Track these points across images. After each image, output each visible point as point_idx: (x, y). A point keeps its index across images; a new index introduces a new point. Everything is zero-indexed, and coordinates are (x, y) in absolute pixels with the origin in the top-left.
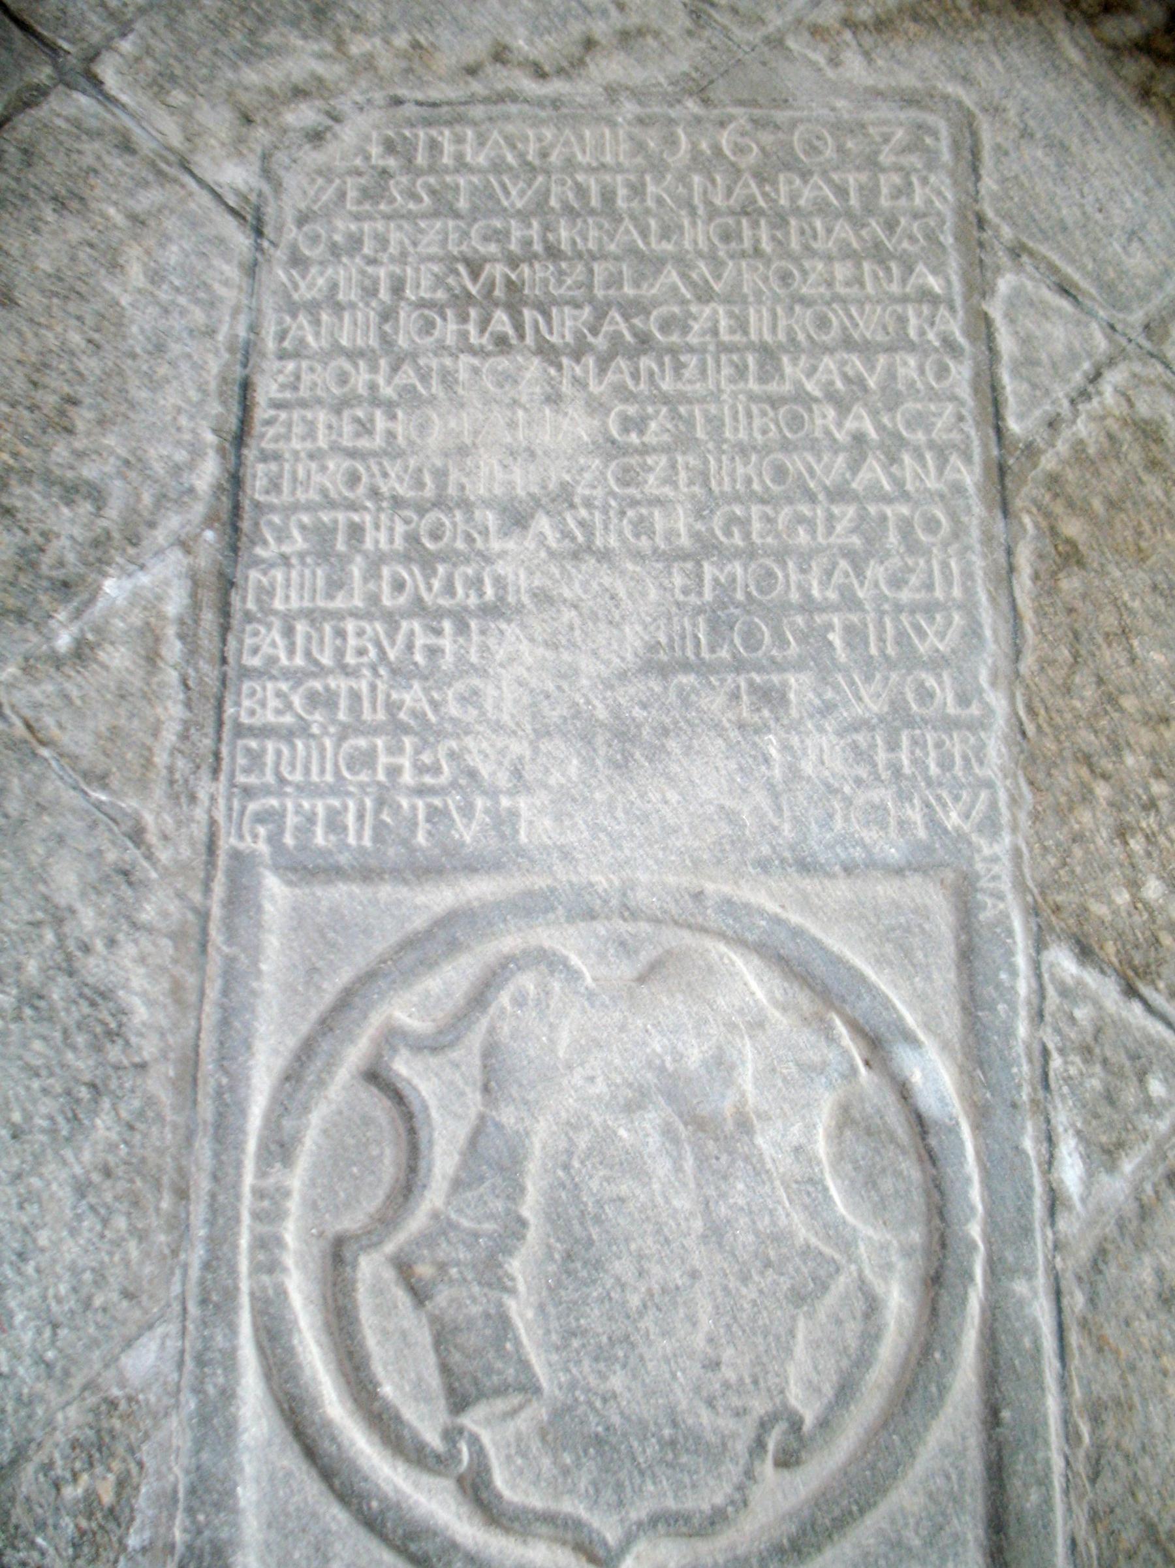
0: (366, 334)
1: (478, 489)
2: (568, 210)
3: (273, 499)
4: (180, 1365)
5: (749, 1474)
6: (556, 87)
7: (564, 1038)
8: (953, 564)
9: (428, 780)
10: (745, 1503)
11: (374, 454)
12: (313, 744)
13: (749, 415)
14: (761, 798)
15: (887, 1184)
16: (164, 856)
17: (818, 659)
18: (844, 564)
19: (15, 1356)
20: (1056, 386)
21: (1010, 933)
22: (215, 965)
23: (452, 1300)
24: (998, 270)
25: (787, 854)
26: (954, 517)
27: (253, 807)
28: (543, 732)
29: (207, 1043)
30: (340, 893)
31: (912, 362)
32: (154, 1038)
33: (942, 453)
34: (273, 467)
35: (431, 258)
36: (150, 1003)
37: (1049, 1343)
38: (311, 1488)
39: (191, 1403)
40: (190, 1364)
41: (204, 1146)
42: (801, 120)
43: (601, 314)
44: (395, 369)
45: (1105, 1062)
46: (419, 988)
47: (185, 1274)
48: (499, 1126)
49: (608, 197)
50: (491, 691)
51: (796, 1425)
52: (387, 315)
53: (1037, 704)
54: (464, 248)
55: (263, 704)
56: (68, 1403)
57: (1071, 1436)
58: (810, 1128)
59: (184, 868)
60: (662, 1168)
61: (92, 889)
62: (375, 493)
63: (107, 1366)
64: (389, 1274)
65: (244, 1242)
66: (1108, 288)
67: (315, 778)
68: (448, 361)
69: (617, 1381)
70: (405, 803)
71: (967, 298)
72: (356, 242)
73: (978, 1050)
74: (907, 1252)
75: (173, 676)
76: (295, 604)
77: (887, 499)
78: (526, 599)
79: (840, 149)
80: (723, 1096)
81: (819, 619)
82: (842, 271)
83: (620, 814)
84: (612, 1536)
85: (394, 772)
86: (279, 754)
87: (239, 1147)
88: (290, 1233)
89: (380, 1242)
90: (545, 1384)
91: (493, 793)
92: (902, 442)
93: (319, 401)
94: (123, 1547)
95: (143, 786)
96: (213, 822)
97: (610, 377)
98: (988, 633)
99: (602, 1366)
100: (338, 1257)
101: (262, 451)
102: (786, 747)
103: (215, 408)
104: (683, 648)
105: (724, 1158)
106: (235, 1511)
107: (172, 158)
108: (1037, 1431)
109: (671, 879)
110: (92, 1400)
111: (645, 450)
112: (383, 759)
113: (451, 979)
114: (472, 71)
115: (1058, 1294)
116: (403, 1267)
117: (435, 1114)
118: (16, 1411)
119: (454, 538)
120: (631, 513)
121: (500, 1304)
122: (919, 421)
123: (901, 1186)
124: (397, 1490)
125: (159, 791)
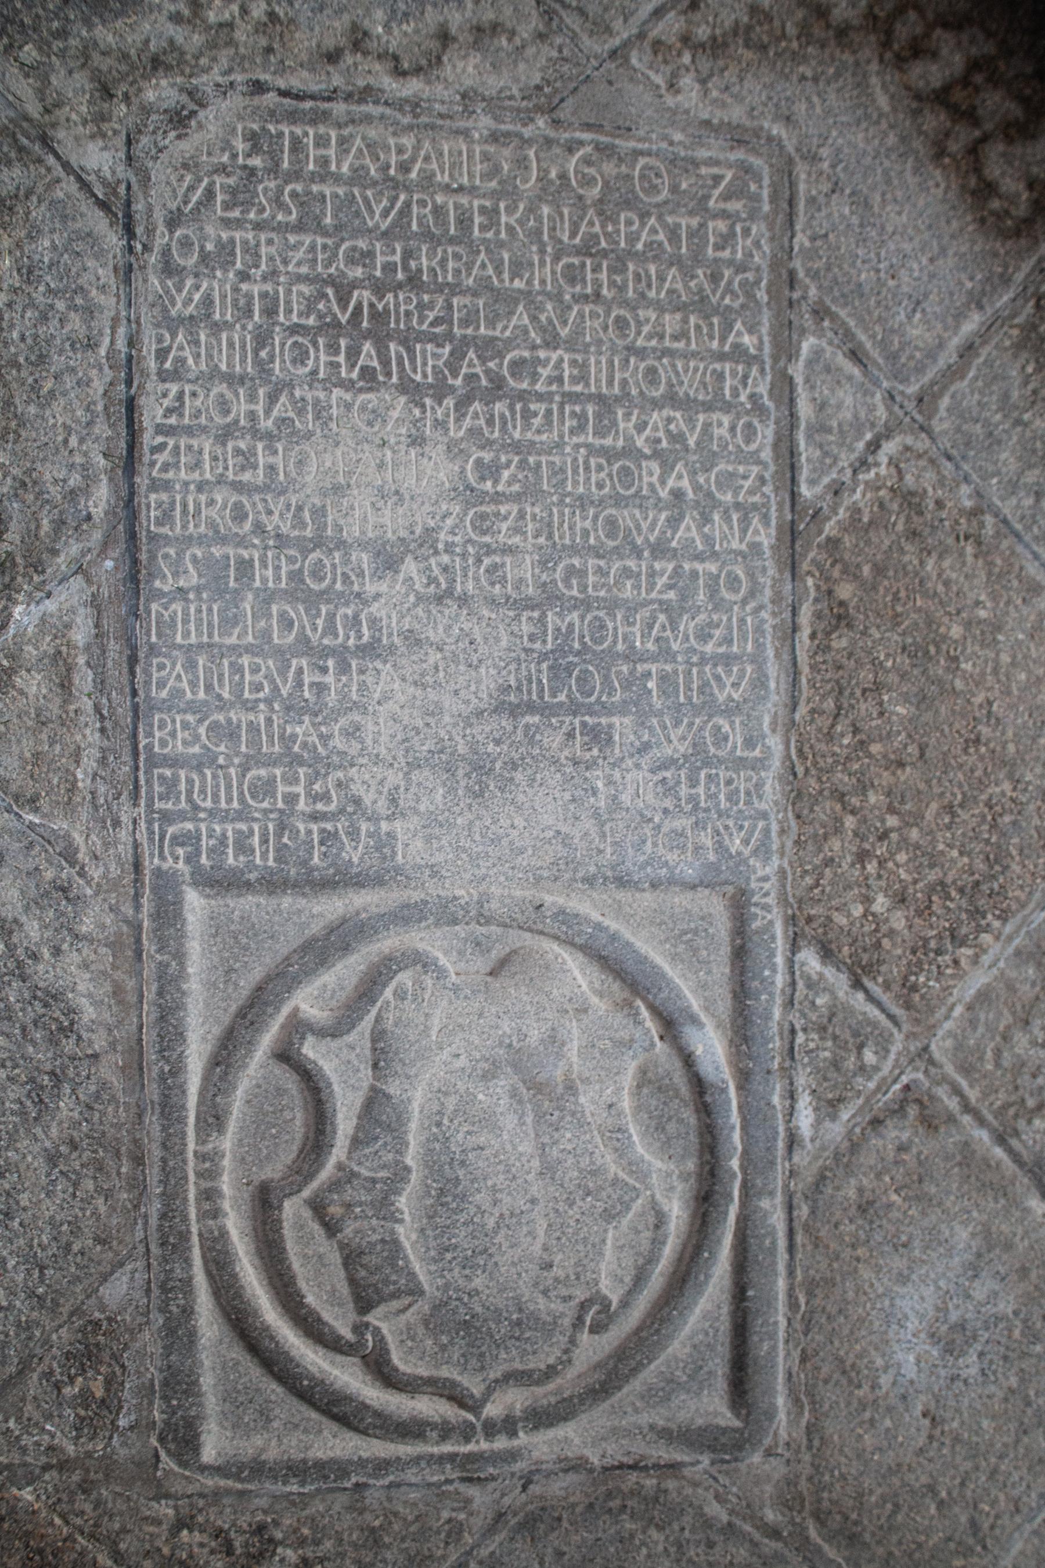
0: (243, 360)
1: (353, 531)
2: (427, 235)
3: (165, 530)
4: (148, 1291)
5: (572, 1341)
6: (413, 87)
7: (436, 1023)
8: (749, 619)
9: (320, 806)
10: (570, 1361)
11: (258, 489)
12: (220, 772)
13: (587, 468)
14: (588, 824)
15: (672, 1127)
16: (96, 873)
17: (637, 705)
18: (662, 618)
19: (11, 1293)
20: (843, 456)
21: (773, 938)
22: (149, 970)
23: (357, 1232)
24: (803, 332)
25: (609, 874)
26: (751, 576)
27: (171, 830)
28: (413, 765)
29: (149, 1036)
30: (248, 903)
31: (726, 420)
32: (102, 1032)
33: (745, 511)
34: (164, 497)
35: (300, 279)
36: (96, 1004)
37: (782, 1243)
38: (254, 1372)
39: (158, 1320)
40: (156, 1292)
41: (153, 1122)
42: (642, 153)
43: (458, 355)
44: (272, 398)
45: (835, 1038)
46: (318, 982)
47: (146, 1224)
48: (388, 1097)
49: (464, 221)
50: (370, 727)
51: (606, 1304)
52: (262, 339)
53: (806, 749)
54: (332, 270)
55: (173, 734)
56: (60, 1326)
57: (793, 1304)
58: (619, 1090)
59: (115, 885)
60: (510, 1122)
61: (34, 903)
62: (259, 528)
63: (88, 1297)
64: (307, 1213)
65: (192, 1196)
66: (893, 357)
67: (223, 805)
68: (322, 395)
69: (478, 1282)
70: (301, 827)
71: (775, 359)
72: (227, 250)
73: (742, 1030)
74: (684, 1177)
75: (88, 705)
76: (193, 639)
77: (699, 557)
78: (396, 640)
79: (674, 189)
80: (556, 1066)
81: (640, 668)
82: (671, 322)
83: (477, 837)
84: (477, 1391)
85: (291, 799)
86: (190, 782)
87: (182, 1121)
88: (226, 1185)
89: (299, 1191)
90: (426, 1287)
91: (374, 819)
92: (716, 504)
93: (204, 429)
94: (115, 1427)
95: (69, 807)
96: (136, 845)
97: (468, 422)
98: (772, 685)
99: (467, 1272)
100: (264, 1202)
101: (153, 480)
102: (610, 782)
103: (101, 429)
104: (529, 692)
105: (556, 1113)
106: (199, 1395)
107: (33, 133)
108: (771, 1302)
109: (518, 893)
110: (79, 1323)
111: (498, 498)
112: (281, 789)
113: (343, 974)
114: (333, 57)
115: (790, 1208)
116: (318, 1207)
117: (336, 1087)
118: (17, 1335)
119: (334, 582)
120: (487, 561)
121: (393, 1232)
122: (728, 480)
123: (683, 1131)
124: (321, 1371)
125: (84, 813)
